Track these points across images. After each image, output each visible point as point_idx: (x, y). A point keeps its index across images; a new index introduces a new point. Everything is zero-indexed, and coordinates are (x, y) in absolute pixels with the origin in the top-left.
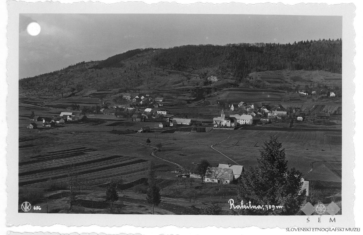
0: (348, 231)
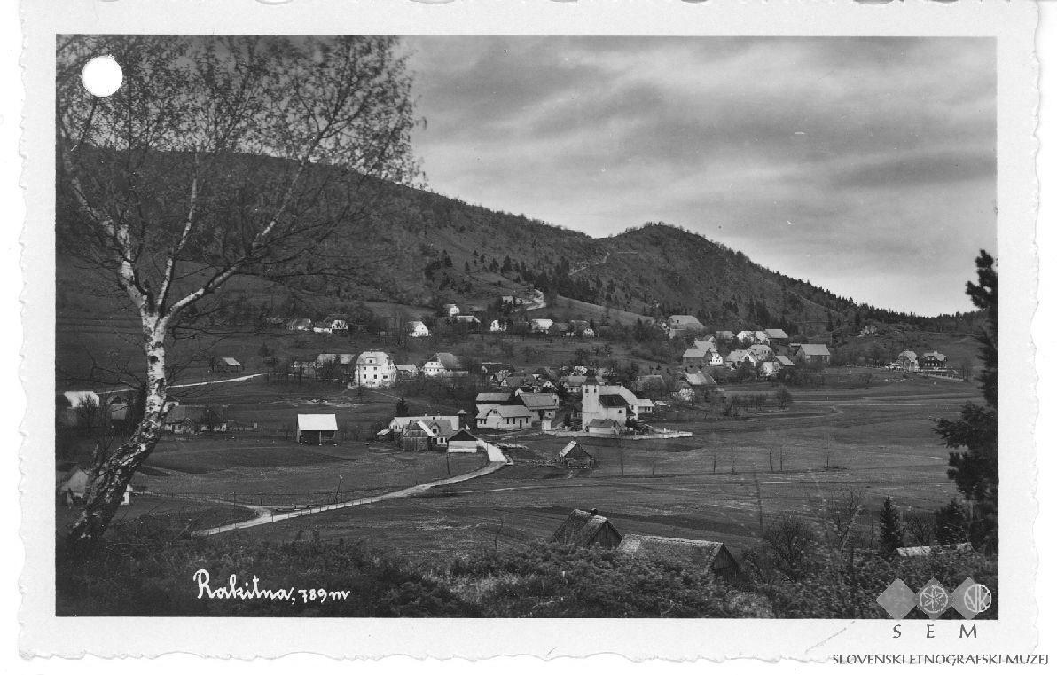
0: (1012, 662)
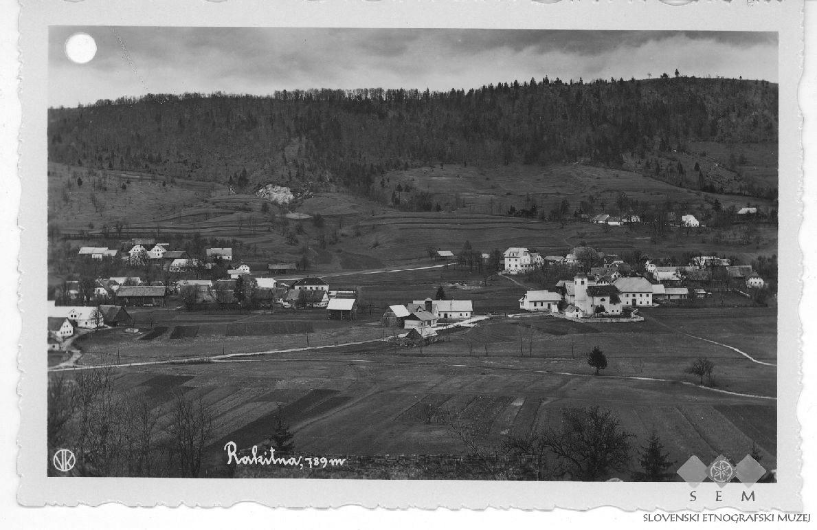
0: (782, 520)
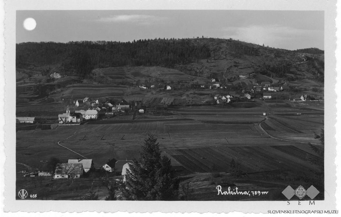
0: (326, 213)
